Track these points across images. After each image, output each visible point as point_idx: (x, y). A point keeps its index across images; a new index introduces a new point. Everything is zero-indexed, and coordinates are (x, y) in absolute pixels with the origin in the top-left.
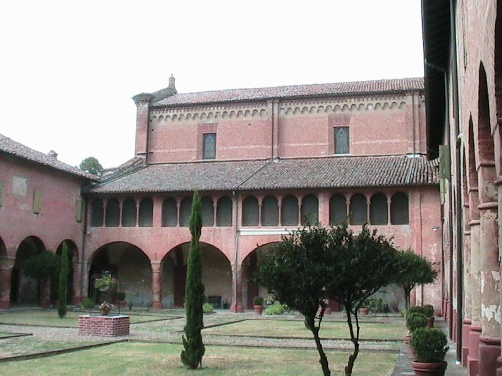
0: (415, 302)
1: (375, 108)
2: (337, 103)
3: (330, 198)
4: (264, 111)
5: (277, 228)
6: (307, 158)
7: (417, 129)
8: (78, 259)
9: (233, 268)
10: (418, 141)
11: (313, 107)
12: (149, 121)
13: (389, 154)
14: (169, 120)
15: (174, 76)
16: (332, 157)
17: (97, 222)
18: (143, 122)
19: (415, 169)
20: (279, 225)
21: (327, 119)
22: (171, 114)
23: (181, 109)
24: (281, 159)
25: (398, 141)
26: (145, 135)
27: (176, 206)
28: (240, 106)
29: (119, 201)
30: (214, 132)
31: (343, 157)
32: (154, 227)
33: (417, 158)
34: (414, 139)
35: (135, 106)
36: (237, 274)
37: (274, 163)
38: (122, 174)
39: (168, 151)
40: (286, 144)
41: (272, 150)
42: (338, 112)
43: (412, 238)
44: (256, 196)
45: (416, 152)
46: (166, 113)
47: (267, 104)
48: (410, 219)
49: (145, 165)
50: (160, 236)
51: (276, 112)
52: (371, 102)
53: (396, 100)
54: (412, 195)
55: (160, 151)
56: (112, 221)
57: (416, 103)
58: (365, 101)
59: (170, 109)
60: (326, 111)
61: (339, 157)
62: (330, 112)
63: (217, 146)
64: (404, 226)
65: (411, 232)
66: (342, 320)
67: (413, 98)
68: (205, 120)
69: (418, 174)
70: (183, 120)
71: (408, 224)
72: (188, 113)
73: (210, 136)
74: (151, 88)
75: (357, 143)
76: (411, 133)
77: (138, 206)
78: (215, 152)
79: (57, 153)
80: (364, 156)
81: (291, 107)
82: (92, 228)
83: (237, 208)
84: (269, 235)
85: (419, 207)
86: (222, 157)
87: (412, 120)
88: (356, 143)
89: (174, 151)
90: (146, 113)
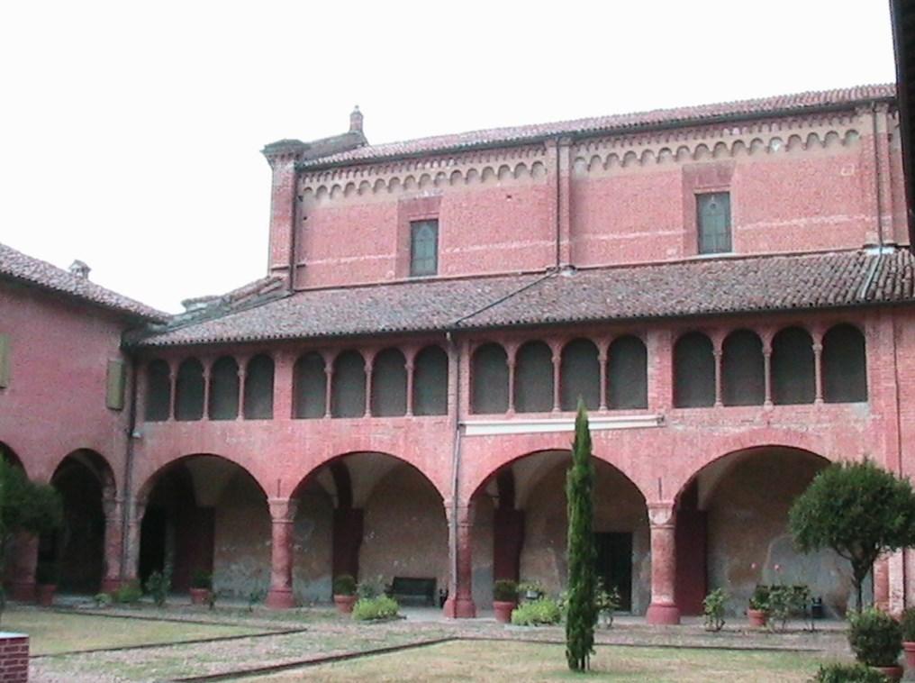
0: (888, 593)
1: (788, 147)
2: (700, 141)
3: (674, 341)
4: (539, 167)
5: (550, 418)
6: (635, 266)
7: (886, 187)
8: (115, 494)
9: (449, 513)
10: (890, 217)
11: (647, 151)
12: (297, 199)
13: (822, 249)
14: (338, 194)
15: (361, 110)
16: (691, 261)
17: (155, 413)
18: (284, 200)
19: (881, 274)
20: (556, 409)
21: (680, 177)
22: (342, 181)
23: (363, 170)
24: (579, 270)
25: (843, 218)
26: (287, 229)
27: (323, 370)
28: (840, 118)
29: (596, 341)
30: (435, 217)
31: (717, 260)
32: (275, 419)
33: (886, 256)
34: (880, 211)
35: (268, 168)
36: (457, 527)
37: (563, 277)
38: (227, 309)
39: (335, 261)
40: (586, 236)
41: (558, 250)
42: (705, 159)
43: (876, 436)
44: (501, 342)
45: (886, 242)
46: (333, 179)
47: (545, 150)
48: (869, 389)
49: (287, 293)
50: (289, 441)
51: (565, 166)
52: (778, 134)
53: (816, 129)
54: (874, 328)
55: (319, 262)
56: (188, 410)
57: (883, 129)
58: (765, 133)
59: (339, 171)
60: (677, 158)
61: (710, 260)
62: (687, 161)
63: (439, 247)
64: (857, 405)
65: (874, 420)
66: (702, 642)
67: (875, 117)
68: (414, 192)
69: (889, 281)
70: (368, 194)
71: (866, 400)
72: (378, 177)
73: (425, 227)
74: (308, 134)
75: (749, 226)
76: (871, 198)
77: (242, 373)
78: (437, 258)
79: (89, 266)
80: (764, 257)
81: (598, 153)
82: (147, 424)
83: (459, 372)
84: (533, 433)
85: (892, 357)
86: (450, 268)
87: (874, 169)
88: (745, 228)
89: (349, 260)
90: (290, 182)
